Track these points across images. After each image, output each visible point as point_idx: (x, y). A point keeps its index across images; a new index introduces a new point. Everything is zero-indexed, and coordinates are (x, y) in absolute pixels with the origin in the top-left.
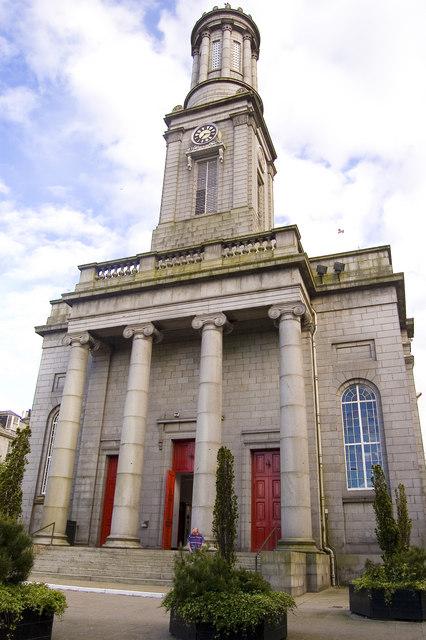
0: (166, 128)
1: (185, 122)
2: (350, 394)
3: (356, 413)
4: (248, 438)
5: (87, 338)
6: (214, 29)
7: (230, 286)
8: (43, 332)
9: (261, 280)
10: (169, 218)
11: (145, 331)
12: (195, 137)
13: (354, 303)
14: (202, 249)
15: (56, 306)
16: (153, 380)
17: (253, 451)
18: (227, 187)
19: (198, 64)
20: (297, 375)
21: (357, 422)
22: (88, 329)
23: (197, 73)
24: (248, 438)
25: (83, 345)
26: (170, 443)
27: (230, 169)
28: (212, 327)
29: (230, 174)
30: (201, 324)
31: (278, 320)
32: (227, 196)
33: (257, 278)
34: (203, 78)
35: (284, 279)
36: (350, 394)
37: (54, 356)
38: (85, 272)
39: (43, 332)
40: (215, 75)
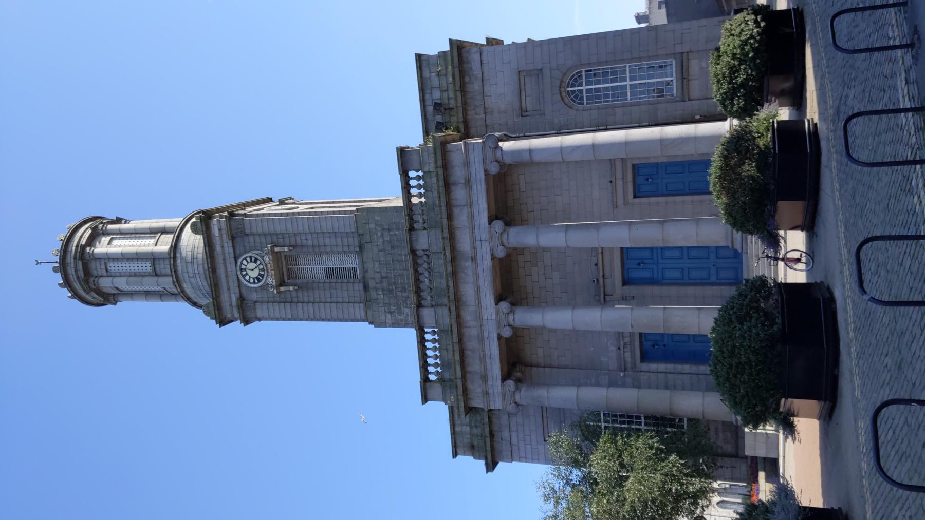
0: (237, 324)
1: (229, 299)
2: (576, 80)
3: (598, 90)
4: (620, 201)
5: (510, 383)
6: (87, 273)
7: (461, 219)
8: (491, 466)
9: (455, 184)
10: (359, 310)
11: (505, 311)
12: (254, 283)
13: (477, 71)
14: (413, 252)
15: (459, 451)
16: (555, 304)
17: (635, 197)
18: (327, 241)
19: (131, 295)
20: (452, 98)
21: (606, 89)
22: (499, 382)
23: (162, 295)
24: (620, 201)
25: (517, 389)
26: (626, 288)
27: (303, 237)
28: (505, 237)
29: (309, 237)
30: (501, 248)
31: (502, 165)
32: (339, 240)
33: (453, 188)
34: (167, 283)
35: (457, 159)
36: (576, 80)
37: (522, 444)
38: (429, 396)
39: (491, 466)
40: (164, 267)
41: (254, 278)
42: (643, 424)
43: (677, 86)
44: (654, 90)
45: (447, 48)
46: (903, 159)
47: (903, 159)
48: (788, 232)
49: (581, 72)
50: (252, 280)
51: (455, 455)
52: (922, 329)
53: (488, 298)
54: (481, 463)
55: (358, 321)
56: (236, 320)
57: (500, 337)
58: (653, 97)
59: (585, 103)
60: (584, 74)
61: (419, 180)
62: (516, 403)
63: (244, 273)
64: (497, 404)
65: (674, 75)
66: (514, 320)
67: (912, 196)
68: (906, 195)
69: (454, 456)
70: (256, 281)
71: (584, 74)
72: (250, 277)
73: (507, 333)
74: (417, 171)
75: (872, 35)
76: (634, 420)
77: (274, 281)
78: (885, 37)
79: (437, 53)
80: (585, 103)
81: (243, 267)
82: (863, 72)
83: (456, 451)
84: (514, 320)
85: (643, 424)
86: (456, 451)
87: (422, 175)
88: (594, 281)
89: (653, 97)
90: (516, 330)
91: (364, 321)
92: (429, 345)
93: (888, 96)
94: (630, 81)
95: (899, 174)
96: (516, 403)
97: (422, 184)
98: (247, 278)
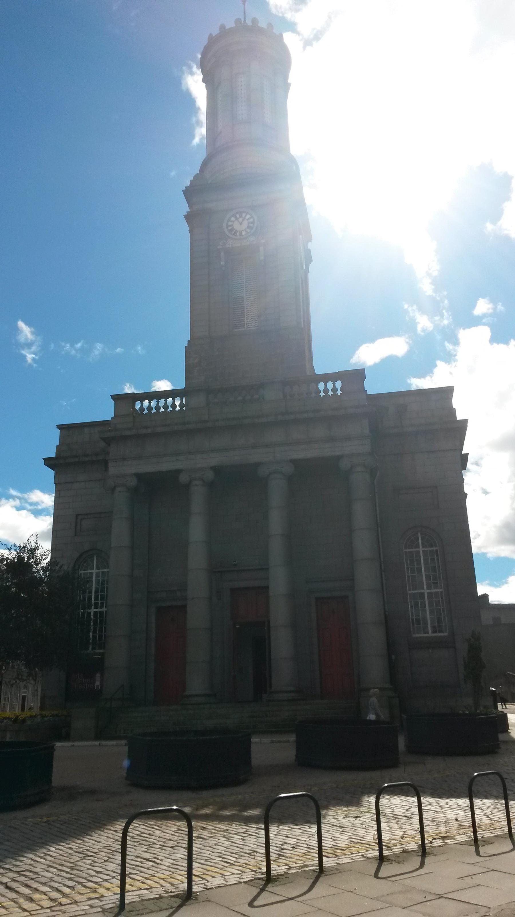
8: (49, 462)
39: (49, 462)
41: (232, 225)
42: (96, 610)
43: (423, 637)
44: (419, 616)
45: (459, 418)
46: (264, 857)
47: (264, 857)
48: (57, 780)
49: (436, 547)
50: (230, 223)
51: (60, 427)
52: (137, 874)
53: (215, 460)
54: (52, 454)
55: (191, 330)
56: (190, 206)
57: (179, 471)
58: (412, 615)
59: (436, 548)
60: (434, 548)
61: (324, 391)
62: (115, 487)
63: (238, 216)
64: (113, 470)
65: (434, 635)
66: (196, 485)
67: (348, 843)
68: (347, 839)
69: (60, 427)
70: (229, 228)
71: (434, 548)
72: (233, 221)
73: (183, 478)
74: (341, 389)
75: (481, 810)
76: (99, 602)
77: (230, 246)
78: (481, 820)
79: (454, 407)
80: (436, 548)
81: (244, 215)
82: (447, 804)
83: (64, 428)
84: (196, 485)
85: (96, 610)
86: (64, 428)
87: (176, 410)
88: (235, 562)
89: (412, 615)
90: (187, 486)
91: (191, 335)
92: (153, 403)
93: (430, 824)
94: (428, 593)
95: (364, 833)
96: (115, 487)
97: (337, 393)
98: (233, 219)
